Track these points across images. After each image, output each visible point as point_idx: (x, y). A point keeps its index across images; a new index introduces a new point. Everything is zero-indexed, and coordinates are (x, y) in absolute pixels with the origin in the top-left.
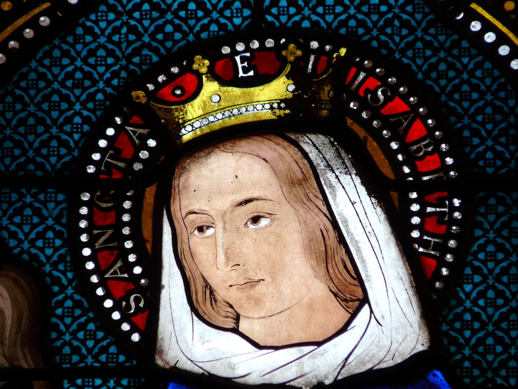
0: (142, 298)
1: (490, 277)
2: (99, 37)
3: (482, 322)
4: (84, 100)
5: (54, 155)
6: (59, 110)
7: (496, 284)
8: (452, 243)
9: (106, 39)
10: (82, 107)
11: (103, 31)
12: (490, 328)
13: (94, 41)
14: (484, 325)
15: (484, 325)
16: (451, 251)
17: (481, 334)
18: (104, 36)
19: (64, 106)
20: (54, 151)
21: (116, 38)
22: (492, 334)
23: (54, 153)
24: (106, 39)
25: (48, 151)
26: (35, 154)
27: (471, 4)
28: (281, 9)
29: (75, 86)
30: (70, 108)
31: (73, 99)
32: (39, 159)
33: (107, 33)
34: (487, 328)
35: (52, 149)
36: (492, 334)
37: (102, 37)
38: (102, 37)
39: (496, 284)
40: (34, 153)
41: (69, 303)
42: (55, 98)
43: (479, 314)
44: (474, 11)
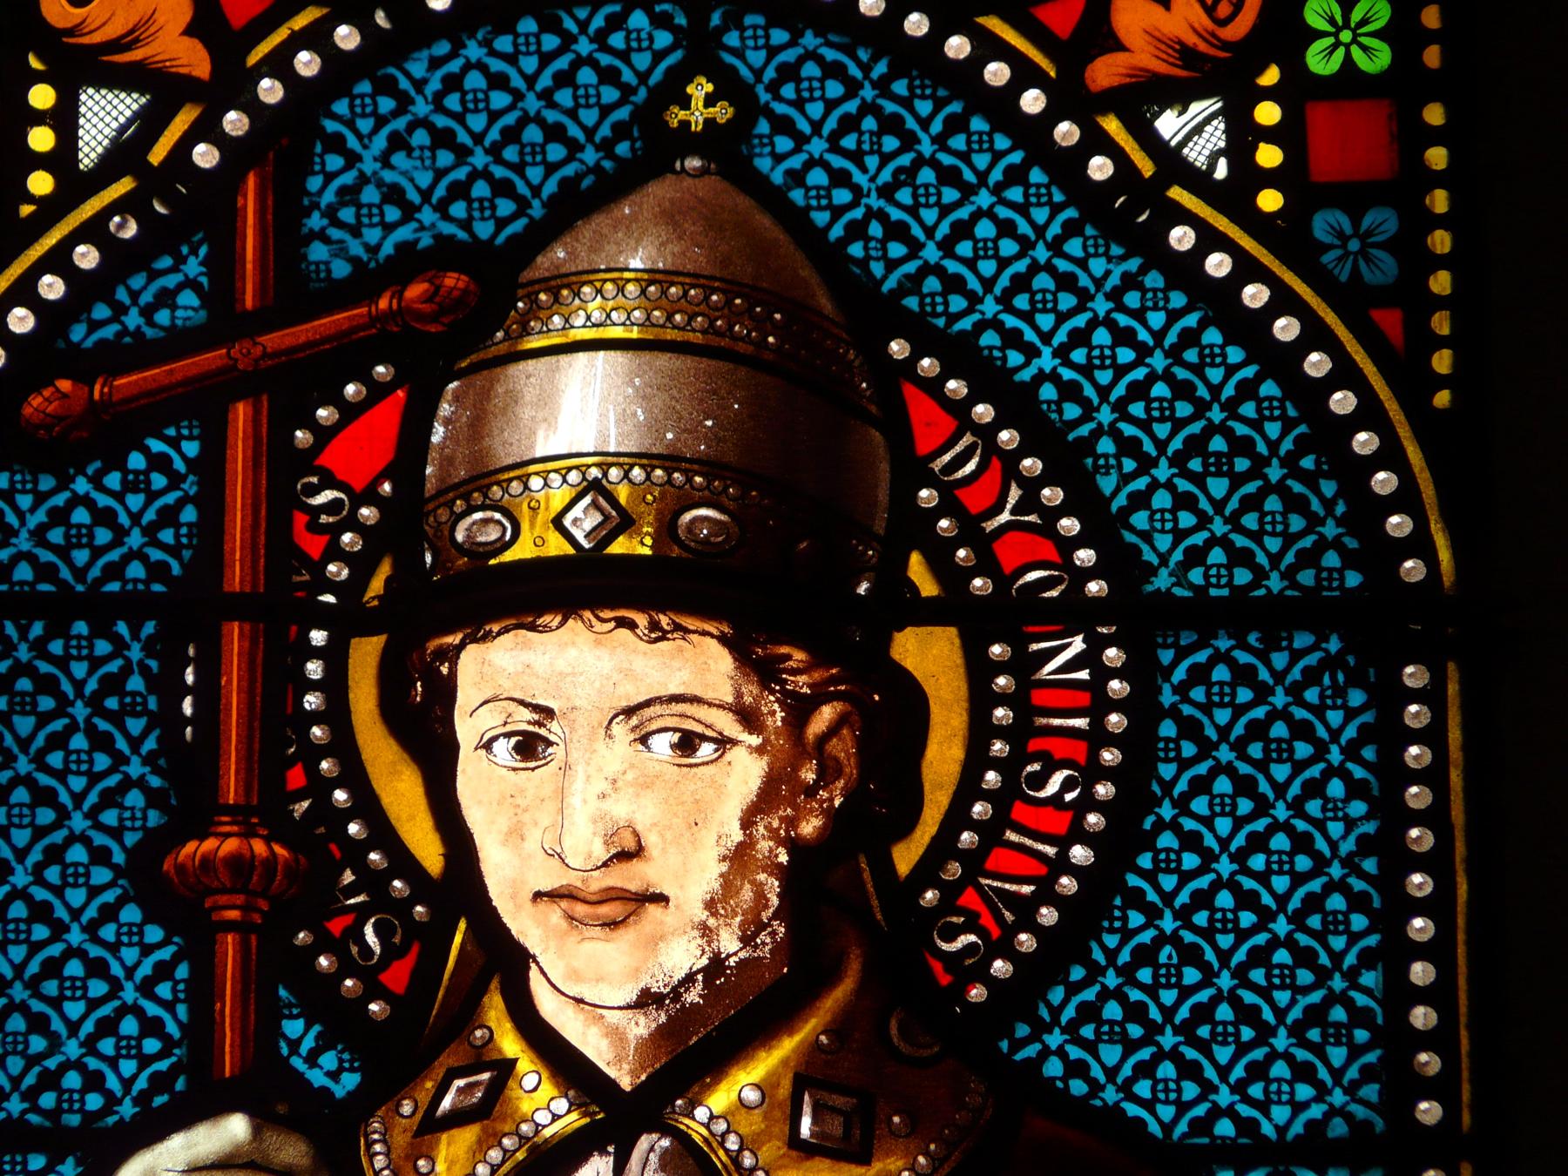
0: (399, 930)
1: (1335, 749)
2: (808, 140)
3: (1316, 856)
4: (151, 523)
5: (79, 658)
6: (90, 545)
7: (1350, 765)
8: (1109, 756)
9: (826, 146)
10: (146, 539)
11: (817, 126)
12: (1336, 871)
13: (797, 150)
14: (1320, 864)
15: (1320, 864)
16: (1107, 774)
17: (1315, 885)
18: (820, 136)
19: (103, 536)
20: (79, 647)
21: (849, 142)
22: (1341, 886)
23: (79, 652)
24: (826, 146)
25: (67, 647)
26: (34, 653)
27: (1168, 187)
28: (975, 138)
29: (129, 487)
30: (117, 542)
31: (124, 519)
32: (44, 667)
33: (826, 131)
34: (1327, 870)
35: (74, 643)
36: (1341, 886)
37: (815, 140)
38: (815, 140)
39: (1350, 765)
40: (30, 650)
41: (1162, 499)
42: (81, 516)
43: (1308, 837)
44: (1176, 205)
